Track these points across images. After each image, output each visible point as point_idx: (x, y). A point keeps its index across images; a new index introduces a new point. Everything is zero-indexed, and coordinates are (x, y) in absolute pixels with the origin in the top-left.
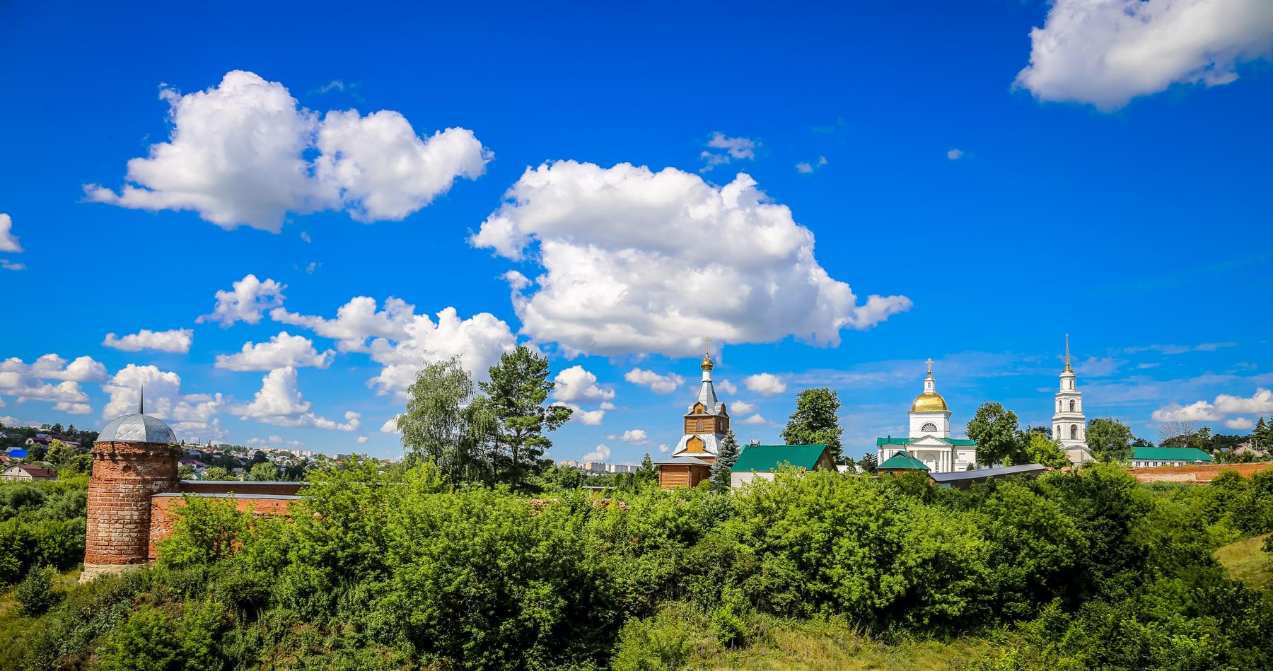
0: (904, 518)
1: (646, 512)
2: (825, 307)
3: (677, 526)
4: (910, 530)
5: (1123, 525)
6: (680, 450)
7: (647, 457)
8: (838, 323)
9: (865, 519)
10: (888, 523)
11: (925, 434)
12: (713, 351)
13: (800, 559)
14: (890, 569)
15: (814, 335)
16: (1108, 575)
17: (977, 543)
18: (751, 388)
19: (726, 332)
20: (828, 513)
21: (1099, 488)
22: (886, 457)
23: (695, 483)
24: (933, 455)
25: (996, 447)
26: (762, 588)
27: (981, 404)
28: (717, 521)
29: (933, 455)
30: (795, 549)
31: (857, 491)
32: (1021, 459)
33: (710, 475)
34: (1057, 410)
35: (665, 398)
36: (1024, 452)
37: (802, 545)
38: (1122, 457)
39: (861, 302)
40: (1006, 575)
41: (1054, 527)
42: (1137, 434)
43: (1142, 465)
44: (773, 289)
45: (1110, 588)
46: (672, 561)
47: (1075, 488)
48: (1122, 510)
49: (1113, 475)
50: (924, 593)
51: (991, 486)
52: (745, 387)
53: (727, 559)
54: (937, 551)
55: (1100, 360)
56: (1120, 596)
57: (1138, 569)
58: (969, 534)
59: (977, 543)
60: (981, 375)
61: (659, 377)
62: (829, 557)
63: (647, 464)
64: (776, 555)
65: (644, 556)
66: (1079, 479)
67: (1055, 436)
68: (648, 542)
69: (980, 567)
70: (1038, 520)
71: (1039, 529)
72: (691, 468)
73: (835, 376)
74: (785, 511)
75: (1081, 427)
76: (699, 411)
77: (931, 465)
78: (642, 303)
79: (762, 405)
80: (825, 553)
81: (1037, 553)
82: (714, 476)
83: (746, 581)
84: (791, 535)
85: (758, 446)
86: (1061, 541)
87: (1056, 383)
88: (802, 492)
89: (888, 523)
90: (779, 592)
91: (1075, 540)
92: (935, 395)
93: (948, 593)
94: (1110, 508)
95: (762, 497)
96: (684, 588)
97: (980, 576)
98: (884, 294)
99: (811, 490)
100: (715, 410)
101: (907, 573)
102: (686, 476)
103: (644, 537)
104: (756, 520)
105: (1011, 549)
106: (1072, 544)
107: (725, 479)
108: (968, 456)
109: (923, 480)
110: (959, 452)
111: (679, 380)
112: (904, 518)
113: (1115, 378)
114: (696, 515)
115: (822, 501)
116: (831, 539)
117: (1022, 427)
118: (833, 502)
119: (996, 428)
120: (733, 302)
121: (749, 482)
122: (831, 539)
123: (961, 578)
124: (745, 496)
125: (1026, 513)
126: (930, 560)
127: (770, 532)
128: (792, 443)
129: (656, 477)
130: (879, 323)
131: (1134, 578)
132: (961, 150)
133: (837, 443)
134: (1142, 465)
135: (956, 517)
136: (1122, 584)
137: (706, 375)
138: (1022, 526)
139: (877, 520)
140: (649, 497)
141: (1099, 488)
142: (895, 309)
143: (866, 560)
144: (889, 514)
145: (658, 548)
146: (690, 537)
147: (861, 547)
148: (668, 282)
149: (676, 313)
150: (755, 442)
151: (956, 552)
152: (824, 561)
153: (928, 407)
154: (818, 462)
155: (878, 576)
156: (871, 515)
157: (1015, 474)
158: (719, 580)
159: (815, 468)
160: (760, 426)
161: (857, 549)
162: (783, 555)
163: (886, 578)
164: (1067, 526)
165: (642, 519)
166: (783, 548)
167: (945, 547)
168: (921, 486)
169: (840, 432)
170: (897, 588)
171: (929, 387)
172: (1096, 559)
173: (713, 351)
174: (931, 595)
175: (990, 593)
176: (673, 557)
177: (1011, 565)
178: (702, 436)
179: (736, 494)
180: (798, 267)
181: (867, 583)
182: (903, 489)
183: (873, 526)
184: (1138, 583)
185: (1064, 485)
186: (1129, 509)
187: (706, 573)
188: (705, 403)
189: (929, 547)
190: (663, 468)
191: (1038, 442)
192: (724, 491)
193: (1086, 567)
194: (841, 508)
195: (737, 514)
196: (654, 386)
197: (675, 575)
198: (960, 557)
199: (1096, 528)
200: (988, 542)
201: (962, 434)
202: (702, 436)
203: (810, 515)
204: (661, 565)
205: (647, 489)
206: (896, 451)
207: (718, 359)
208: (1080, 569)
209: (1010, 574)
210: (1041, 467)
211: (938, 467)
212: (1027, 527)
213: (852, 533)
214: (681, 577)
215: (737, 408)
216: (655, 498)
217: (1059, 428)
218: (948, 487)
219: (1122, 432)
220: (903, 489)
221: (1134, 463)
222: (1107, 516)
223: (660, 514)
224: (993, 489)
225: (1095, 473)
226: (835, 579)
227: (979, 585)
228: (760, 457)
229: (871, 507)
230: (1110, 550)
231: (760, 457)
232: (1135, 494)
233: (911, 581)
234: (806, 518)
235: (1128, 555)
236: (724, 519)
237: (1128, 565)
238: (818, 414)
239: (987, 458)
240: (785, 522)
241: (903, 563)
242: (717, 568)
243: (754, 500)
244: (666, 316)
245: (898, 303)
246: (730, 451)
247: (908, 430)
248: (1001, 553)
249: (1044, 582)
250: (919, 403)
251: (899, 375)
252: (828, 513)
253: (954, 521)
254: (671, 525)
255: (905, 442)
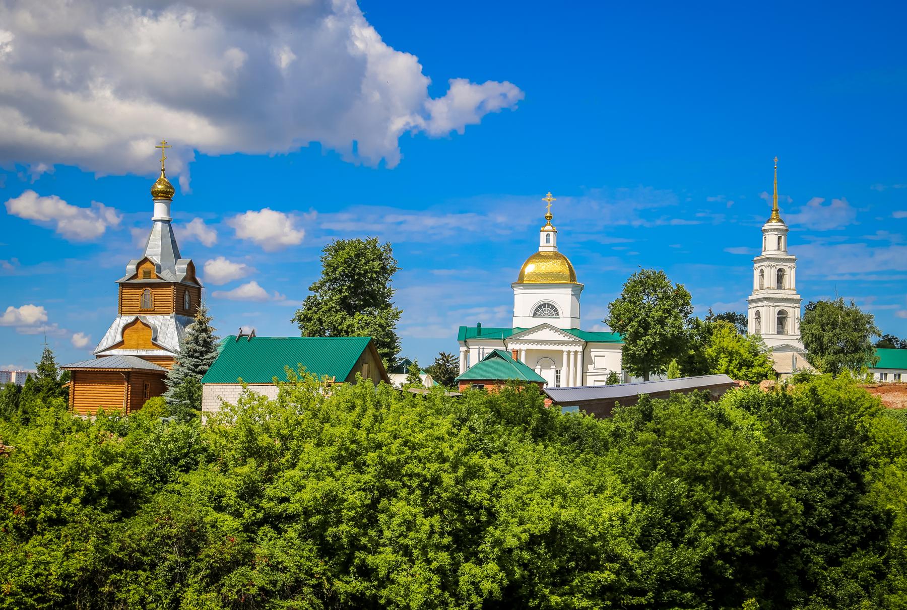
0: (500, 463)
1: (42, 456)
2: (377, 96)
3: (100, 482)
4: (509, 486)
5: (856, 478)
6: (111, 343)
7: (48, 356)
8: (398, 124)
9: (434, 467)
10: (473, 473)
11: (539, 321)
12: (176, 166)
13: (322, 537)
14: (475, 554)
15: (355, 143)
16: (833, 561)
17: (620, 507)
18: (241, 234)
19: (198, 131)
20: (371, 457)
21: (820, 417)
22: (474, 360)
23: (136, 403)
24: (551, 358)
25: (655, 346)
26: (253, 591)
27: (630, 272)
28: (175, 472)
29: (551, 358)
30: (314, 520)
31: (422, 417)
32: (695, 366)
33: (164, 389)
34: (756, 285)
35: (85, 249)
36: (700, 355)
37: (326, 513)
38: (857, 365)
39: (438, 90)
40: (667, 562)
41: (747, 480)
42: (882, 326)
43: (890, 378)
44: (285, 58)
45: (836, 583)
46: (90, 547)
47: (781, 412)
48: (855, 453)
49: (842, 394)
50: (533, 595)
51: (645, 410)
52: (232, 232)
53: (192, 540)
54: (555, 521)
55: (827, 204)
56: (851, 596)
57: (881, 551)
58: (608, 493)
59: (620, 507)
60: (636, 223)
61: (72, 210)
62: (372, 533)
63: (47, 369)
64: (279, 531)
65: (36, 539)
66: (789, 401)
67: (751, 328)
68: (44, 512)
69: (624, 549)
70: (720, 468)
71: (724, 484)
72: (130, 376)
73: (390, 218)
74: (296, 454)
75: (795, 314)
76: (147, 274)
77: (548, 375)
78: (43, 70)
79: (260, 263)
80: (365, 527)
81: (718, 523)
82: (172, 390)
83: (225, 580)
84: (306, 495)
85: (252, 338)
86: (757, 504)
87: (757, 244)
88: (326, 420)
89: (473, 473)
90: (286, 598)
91: (779, 503)
92: (556, 256)
93: (572, 593)
94: (836, 450)
95: (256, 428)
96: (111, 594)
97: (625, 564)
98: (477, 79)
99: (343, 416)
100: (177, 272)
101: (505, 558)
102: (119, 393)
103: (38, 503)
104: (246, 469)
105: (676, 519)
106: (774, 507)
107: (193, 398)
108: (610, 360)
109: (533, 400)
110: (594, 352)
111: (112, 217)
112: (500, 463)
113: (852, 234)
114: (136, 462)
115: (362, 435)
116: (375, 502)
117: (699, 312)
118: (381, 437)
119: (656, 314)
120: (212, 79)
121: (234, 402)
122: (375, 502)
123: (595, 566)
124: (226, 426)
125: (701, 456)
126: (543, 536)
127: (269, 490)
128: (312, 334)
129: (65, 393)
130: (468, 127)
131: (874, 567)
132: (522, 88)
133: (391, 335)
134: (890, 378)
135: (586, 462)
136: (855, 576)
137: (160, 210)
138: (694, 478)
139: (455, 468)
140: (48, 430)
141: (820, 417)
142: (494, 105)
143: (436, 537)
144: (475, 459)
145: (62, 522)
146: (124, 502)
147: (427, 515)
148: (91, 34)
149: (108, 93)
150: (247, 331)
151: (584, 523)
152: (364, 540)
153: (546, 275)
154: (357, 367)
155: (456, 566)
156: (444, 460)
157: (685, 391)
158: (177, 578)
159: (350, 378)
160: (254, 303)
161: (420, 519)
162: (292, 531)
163: (468, 568)
164: (767, 478)
165: (34, 470)
166: (291, 518)
167: (567, 514)
168: (526, 413)
169: (396, 316)
170: (486, 586)
171: (547, 242)
172: (812, 534)
173: (176, 166)
174: (544, 598)
175: (642, 593)
176: (93, 539)
177: (675, 545)
178: (151, 320)
179: (211, 422)
180: (330, 23)
181: (436, 579)
182: (499, 414)
183: (448, 479)
184: (880, 575)
185: (764, 410)
186: (868, 451)
187: (153, 566)
188: (157, 260)
189: (541, 514)
190: (78, 376)
191: (725, 338)
192: (189, 418)
193: (798, 548)
194: (394, 448)
195: (211, 459)
196: (62, 224)
197: (95, 572)
198: (591, 531)
199: (813, 483)
200: (638, 507)
201: (599, 320)
202: (151, 320)
203: (340, 461)
204: (67, 554)
205: (45, 416)
206: (489, 350)
207: (184, 181)
208: (787, 550)
209: (674, 560)
210: (726, 379)
211: (562, 379)
212: (701, 480)
213: (411, 491)
214: (106, 575)
215: (217, 269)
216: (60, 432)
217: (758, 314)
218: (575, 411)
219: (858, 323)
220: (499, 414)
221: (877, 376)
222: (832, 463)
223: (70, 459)
224: (648, 416)
225: (813, 390)
226: (382, 573)
227: (624, 579)
228: (253, 358)
229: (445, 446)
230: (835, 520)
231: (253, 358)
232: (878, 427)
233: (510, 574)
234: (332, 465)
235: (864, 528)
236: (187, 469)
237: (863, 544)
238: (359, 284)
239: (640, 364)
240: (296, 473)
241: (497, 543)
242: (174, 557)
243: (242, 434)
244: (87, 96)
245: (499, 94)
246: (201, 348)
247: (511, 313)
248: (661, 524)
249: (729, 573)
250: (530, 268)
251: (501, 219)
252: (371, 457)
253: (583, 471)
254: (88, 480)
255: (505, 334)
